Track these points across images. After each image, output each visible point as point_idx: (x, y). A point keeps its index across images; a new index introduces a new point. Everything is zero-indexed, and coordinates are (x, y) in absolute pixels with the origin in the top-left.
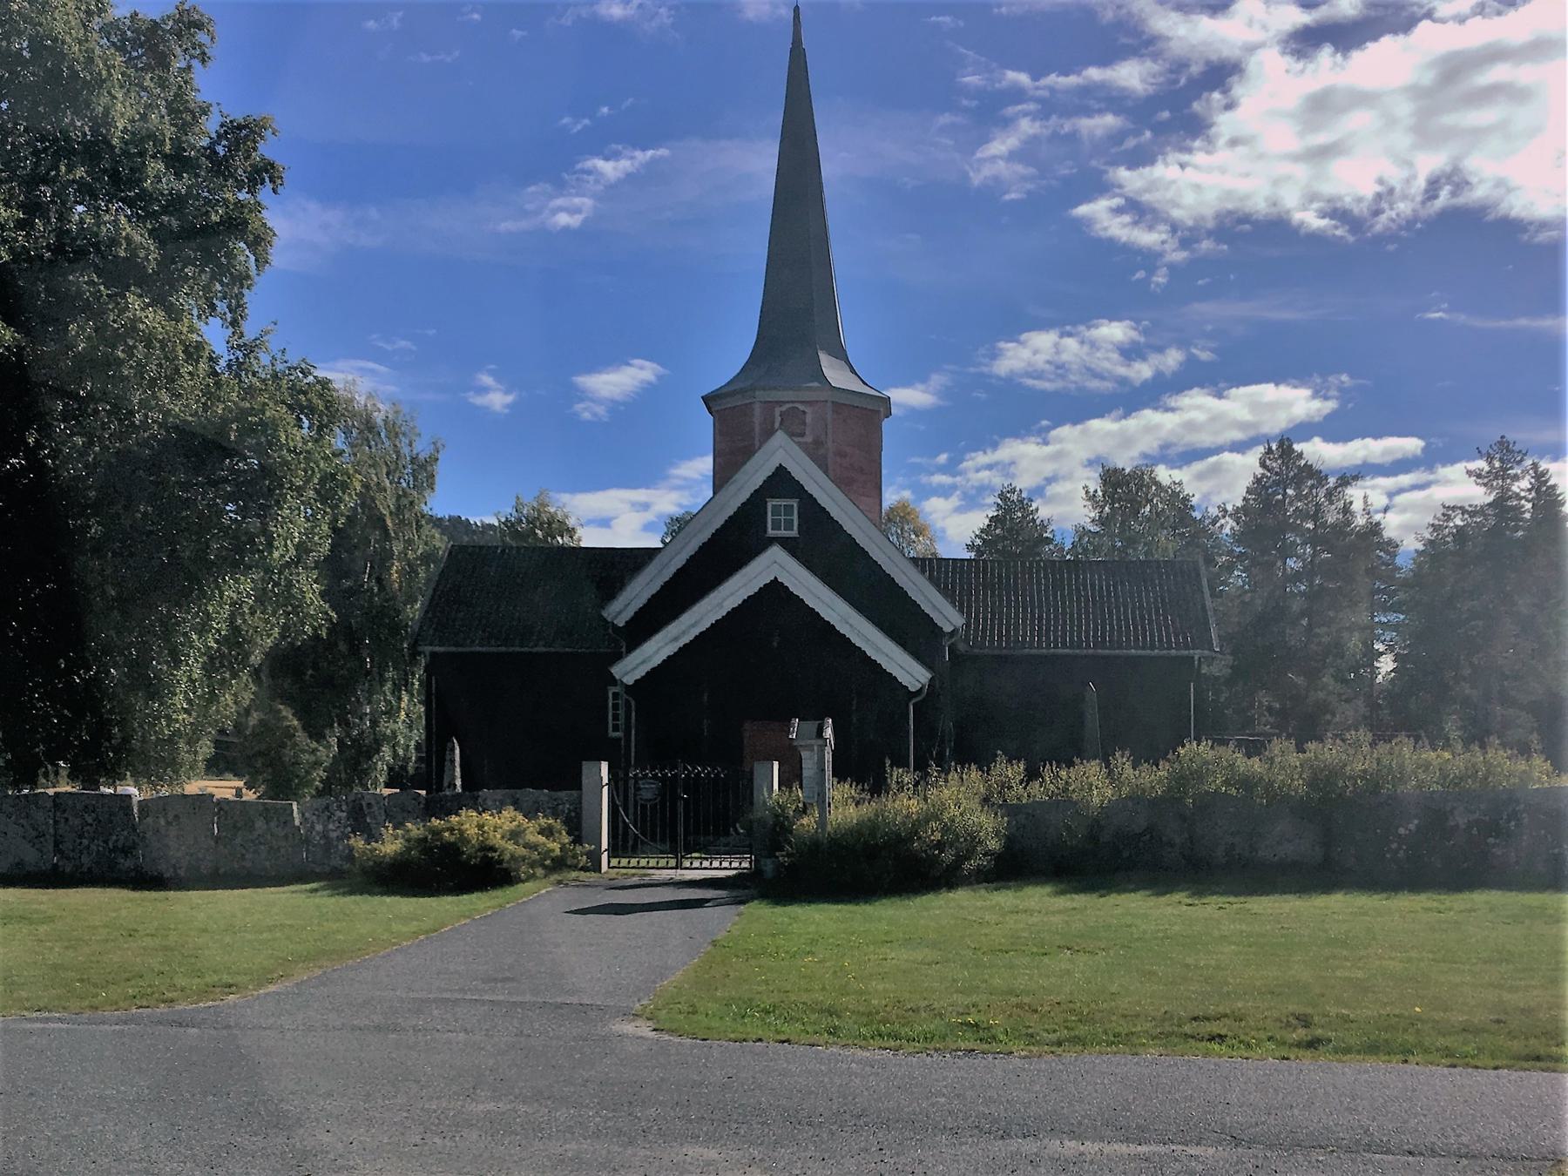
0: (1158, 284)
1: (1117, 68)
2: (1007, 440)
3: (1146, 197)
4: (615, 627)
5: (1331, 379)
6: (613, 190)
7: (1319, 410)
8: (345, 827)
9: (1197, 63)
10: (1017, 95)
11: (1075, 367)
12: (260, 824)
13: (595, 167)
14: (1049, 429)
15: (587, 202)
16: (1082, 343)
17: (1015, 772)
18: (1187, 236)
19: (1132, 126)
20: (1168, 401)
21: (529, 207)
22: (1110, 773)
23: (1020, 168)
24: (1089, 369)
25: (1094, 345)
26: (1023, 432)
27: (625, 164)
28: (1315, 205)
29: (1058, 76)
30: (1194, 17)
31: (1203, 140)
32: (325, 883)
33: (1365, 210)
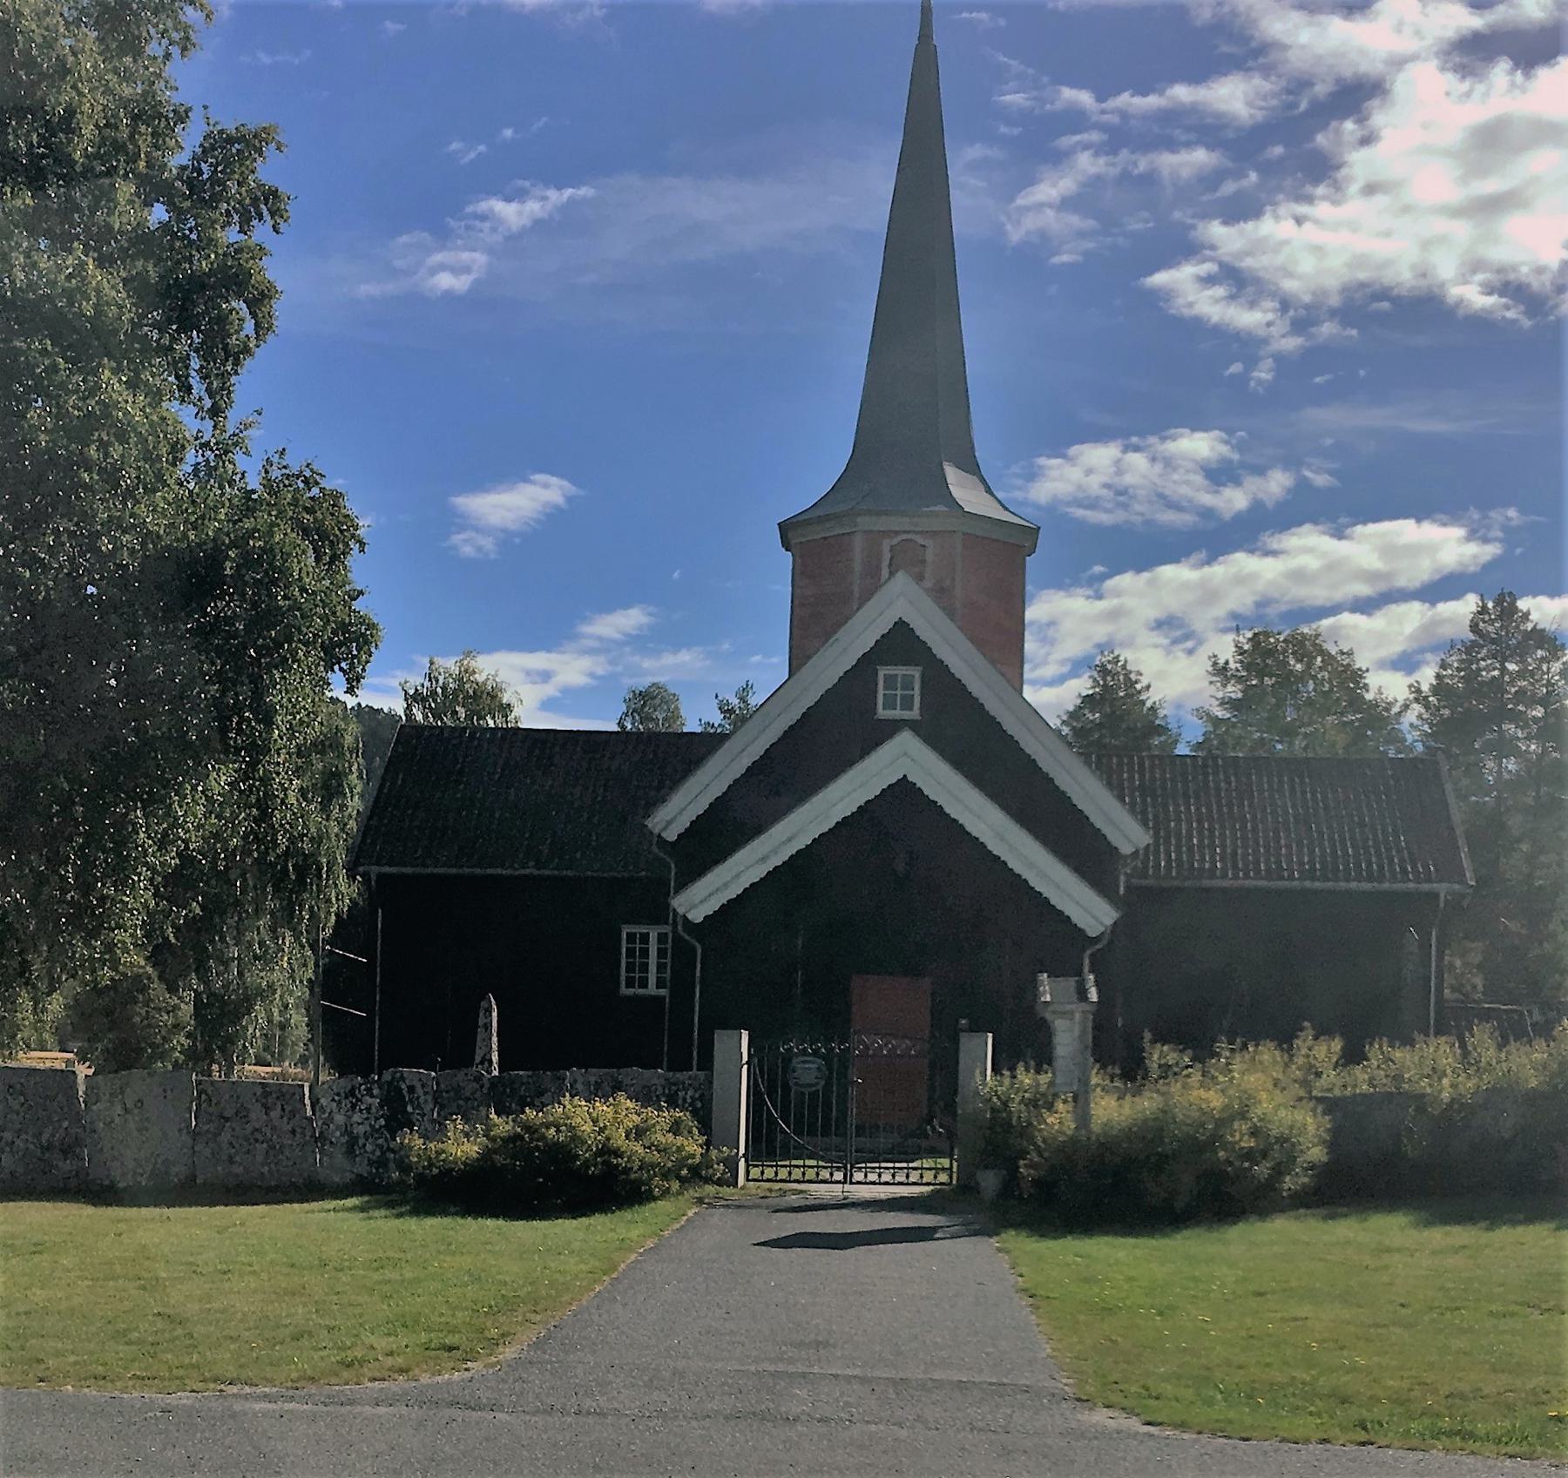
0: (1260, 382)
1: (1215, 86)
2: (1045, 591)
3: (1248, 262)
4: (662, 842)
5: (1493, 514)
6: (515, 242)
7: (1475, 557)
8: (377, 1119)
9: (1323, 81)
10: (1075, 120)
11: (1141, 492)
12: (257, 1114)
13: (491, 210)
14: (1104, 577)
15: (480, 258)
16: (1153, 460)
17: (1328, 1050)
18: (1302, 317)
19: (1230, 165)
20: (1269, 540)
21: (398, 263)
22: (1466, 1054)
23: (1075, 221)
24: (1161, 496)
25: (1169, 463)
26: (1067, 581)
27: (533, 207)
28: (1480, 277)
29: (1133, 96)
30: (1322, 18)
31: (1328, 186)
32: (366, 1198)
33: (1548, 284)
